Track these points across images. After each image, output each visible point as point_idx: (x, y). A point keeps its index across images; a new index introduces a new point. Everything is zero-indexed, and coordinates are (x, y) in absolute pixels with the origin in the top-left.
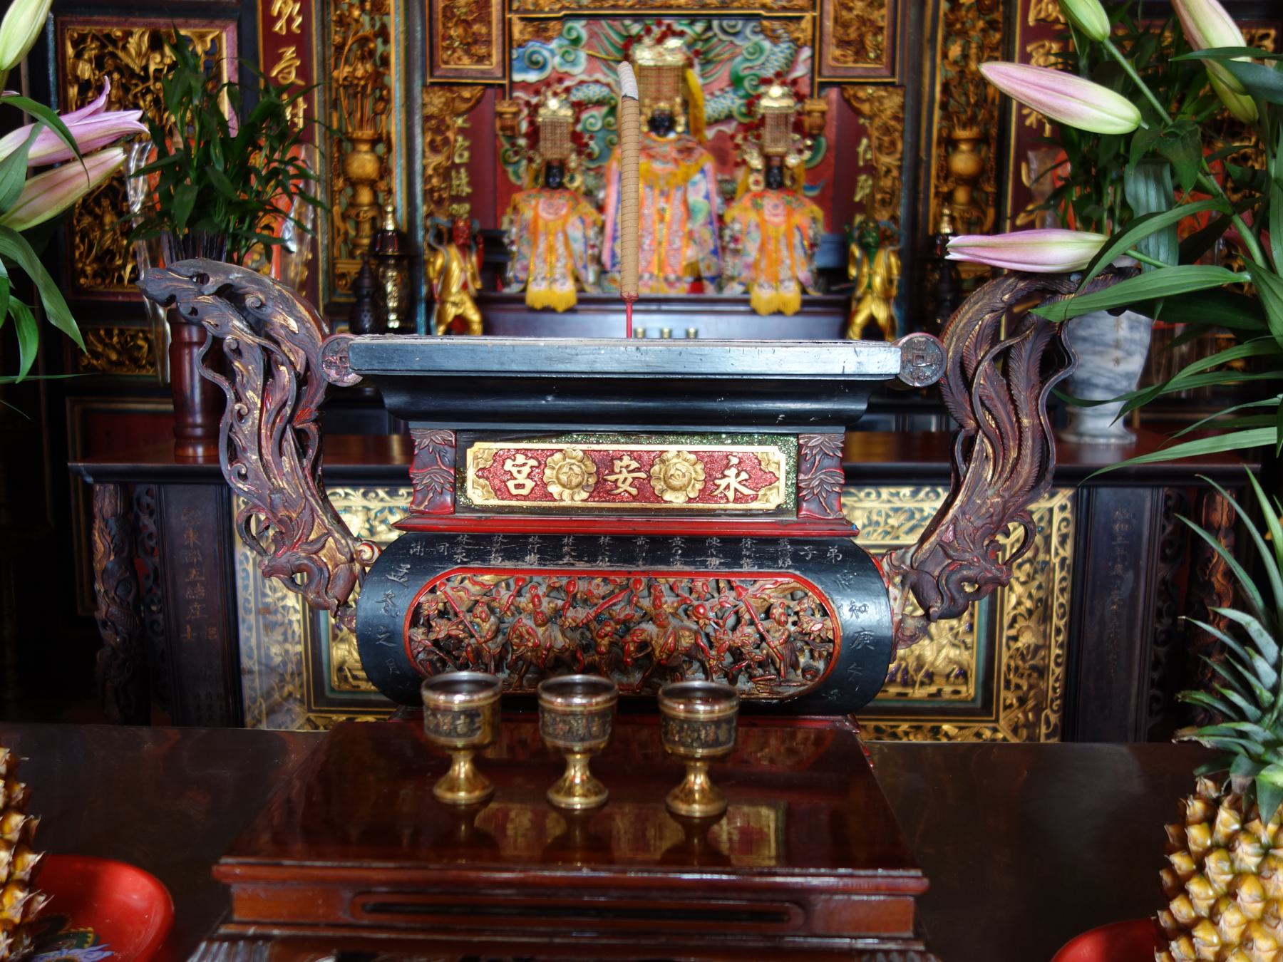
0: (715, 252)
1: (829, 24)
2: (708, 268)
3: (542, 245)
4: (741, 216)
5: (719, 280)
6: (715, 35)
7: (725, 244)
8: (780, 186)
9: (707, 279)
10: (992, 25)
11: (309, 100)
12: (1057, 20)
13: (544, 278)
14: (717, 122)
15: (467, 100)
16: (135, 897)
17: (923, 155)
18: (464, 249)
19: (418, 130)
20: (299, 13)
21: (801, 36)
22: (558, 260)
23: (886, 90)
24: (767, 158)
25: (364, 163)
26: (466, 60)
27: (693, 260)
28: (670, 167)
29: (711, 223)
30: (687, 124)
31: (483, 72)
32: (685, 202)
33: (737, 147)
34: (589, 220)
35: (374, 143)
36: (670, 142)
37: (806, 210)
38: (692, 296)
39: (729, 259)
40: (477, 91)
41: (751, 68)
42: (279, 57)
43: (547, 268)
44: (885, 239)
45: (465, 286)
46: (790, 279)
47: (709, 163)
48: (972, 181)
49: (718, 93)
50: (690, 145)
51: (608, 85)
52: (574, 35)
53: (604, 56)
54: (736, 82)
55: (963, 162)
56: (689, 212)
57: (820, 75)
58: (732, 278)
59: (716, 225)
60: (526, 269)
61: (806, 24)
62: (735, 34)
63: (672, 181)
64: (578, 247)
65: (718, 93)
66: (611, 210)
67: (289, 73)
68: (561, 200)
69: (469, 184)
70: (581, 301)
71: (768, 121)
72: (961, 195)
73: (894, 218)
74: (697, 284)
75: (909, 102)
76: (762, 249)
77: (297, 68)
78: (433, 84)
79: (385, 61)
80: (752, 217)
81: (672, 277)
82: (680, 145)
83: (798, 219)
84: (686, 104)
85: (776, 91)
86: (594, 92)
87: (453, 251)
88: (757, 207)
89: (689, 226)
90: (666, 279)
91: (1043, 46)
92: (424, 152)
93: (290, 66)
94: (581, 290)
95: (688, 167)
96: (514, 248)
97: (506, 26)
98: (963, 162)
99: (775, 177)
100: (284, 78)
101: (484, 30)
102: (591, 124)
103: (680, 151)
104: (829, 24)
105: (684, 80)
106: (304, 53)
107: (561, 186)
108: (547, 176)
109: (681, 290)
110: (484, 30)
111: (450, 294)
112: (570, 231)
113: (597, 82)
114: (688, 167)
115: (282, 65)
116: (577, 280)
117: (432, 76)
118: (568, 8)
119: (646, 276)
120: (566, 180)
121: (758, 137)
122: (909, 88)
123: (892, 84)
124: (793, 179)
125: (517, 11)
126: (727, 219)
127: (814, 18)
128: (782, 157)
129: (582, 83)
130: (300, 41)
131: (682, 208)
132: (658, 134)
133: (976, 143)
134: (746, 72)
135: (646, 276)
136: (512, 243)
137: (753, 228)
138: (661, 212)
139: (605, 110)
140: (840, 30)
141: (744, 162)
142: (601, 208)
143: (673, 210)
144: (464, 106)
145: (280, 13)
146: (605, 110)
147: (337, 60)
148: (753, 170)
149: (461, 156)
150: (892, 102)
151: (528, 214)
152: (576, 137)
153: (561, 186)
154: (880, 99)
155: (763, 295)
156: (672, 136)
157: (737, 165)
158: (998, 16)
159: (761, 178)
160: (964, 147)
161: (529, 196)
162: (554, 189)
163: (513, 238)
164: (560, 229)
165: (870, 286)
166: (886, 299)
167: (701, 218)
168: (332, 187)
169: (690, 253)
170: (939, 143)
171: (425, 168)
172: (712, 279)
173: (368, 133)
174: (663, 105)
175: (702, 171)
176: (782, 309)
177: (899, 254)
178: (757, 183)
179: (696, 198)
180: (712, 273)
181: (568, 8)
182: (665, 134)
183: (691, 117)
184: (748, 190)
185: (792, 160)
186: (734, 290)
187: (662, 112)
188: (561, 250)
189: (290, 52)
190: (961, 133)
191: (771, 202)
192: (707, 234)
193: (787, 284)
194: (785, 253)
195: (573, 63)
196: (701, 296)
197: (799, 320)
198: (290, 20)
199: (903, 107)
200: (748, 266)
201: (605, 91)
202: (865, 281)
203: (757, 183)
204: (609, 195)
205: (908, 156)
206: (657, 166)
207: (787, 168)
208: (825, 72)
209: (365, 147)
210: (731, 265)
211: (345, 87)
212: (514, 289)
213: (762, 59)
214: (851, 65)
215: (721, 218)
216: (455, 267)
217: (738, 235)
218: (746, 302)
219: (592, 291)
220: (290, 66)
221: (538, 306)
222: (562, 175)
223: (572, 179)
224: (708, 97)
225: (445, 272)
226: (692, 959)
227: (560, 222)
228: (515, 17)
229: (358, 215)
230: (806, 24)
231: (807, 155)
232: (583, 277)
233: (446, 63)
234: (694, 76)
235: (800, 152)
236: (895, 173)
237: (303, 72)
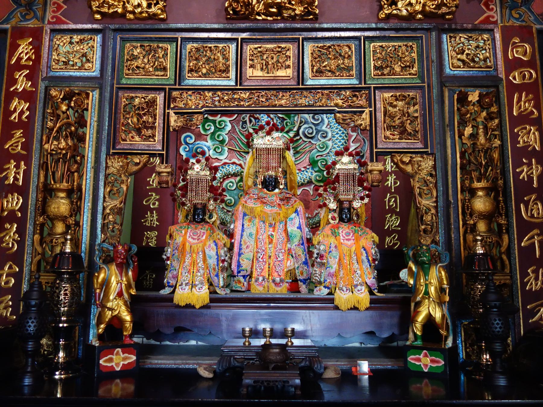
0: (306, 263)
1: (380, 116)
2: (302, 273)
3: (188, 261)
4: (324, 240)
5: (309, 281)
6: (301, 138)
7: (312, 255)
8: (350, 220)
9: (301, 281)
10: (490, 117)
11: (28, 164)
12: (532, 113)
13: (187, 284)
14: (302, 185)
15: (137, 164)
16: (266, 239)
17: (451, 199)
18: (122, 267)
19: (102, 183)
20: (27, 109)
21: (362, 122)
22: (198, 271)
23: (422, 157)
24: (340, 203)
25: (61, 205)
26: (137, 138)
27: (292, 268)
28: (276, 209)
29: (303, 244)
30: (286, 184)
31: (148, 146)
32: (286, 230)
33: (320, 195)
34: (221, 243)
35: (69, 193)
36: (276, 194)
37: (369, 236)
38: (292, 296)
39: (317, 269)
40: (144, 158)
41: (322, 156)
42: (12, 136)
43: (190, 277)
44: (435, 260)
45: (120, 294)
46: (361, 285)
47: (301, 208)
48: (488, 217)
49: (303, 169)
50: (288, 196)
51: (240, 165)
52: (221, 138)
53: (238, 150)
54: (313, 163)
55: (481, 204)
56: (289, 237)
57: (376, 148)
58: (320, 283)
59: (306, 245)
60: (176, 277)
61: (366, 116)
62: (312, 138)
63: (277, 219)
64: (212, 262)
65: (303, 169)
66: (237, 237)
67: (17, 146)
68: (203, 231)
69: (158, 220)
70: (212, 300)
71: (341, 178)
72: (482, 226)
73: (434, 242)
74: (294, 286)
75: (439, 164)
76: (340, 263)
77: (22, 143)
78: (114, 154)
79: (82, 139)
80: (332, 240)
81: (278, 280)
82: (281, 196)
83: (363, 242)
84: (285, 173)
85: (346, 159)
86: (232, 169)
87: (114, 267)
88: (335, 234)
89: (289, 246)
90: (274, 281)
91: (526, 128)
92: (104, 197)
93: (18, 142)
94: (213, 292)
95: (287, 209)
96: (169, 262)
97: (166, 118)
98: (481, 204)
99: (345, 214)
100: (13, 149)
101: (150, 120)
102: (230, 186)
103: (281, 200)
104: (380, 116)
105: (284, 158)
106: (28, 134)
107: (203, 220)
108: (194, 216)
109: (283, 290)
110: (150, 120)
111: (108, 301)
112: (207, 251)
113: (234, 163)
114: (287, 209)
115: (13, 141)
116: (211, 284)
117: (114, 148)
118: (207, 107)
119: (261, 279)
120: (207, 217)
121: (334, 189)
122: (438, 155)
123: (426, 153)
124: (358, 215)
125: (173, 109)
126: (315, 242)
127: (371, 112)
128: (350, 202)
129: (225, 164)
130: (26, 127)
131: (284, 235)
132: (268, 190)
133: (488, 191)
134: (319, 158)
135: (261, 279)
136: (168, 259)
137: (333, 248)
138: (271, 237)
139: (238, 178)
140: (388, 120)
141: (325, 205)
142: (231, 235)
143: (279, 235)
144: (135, 168)
145: (15, 109)
146: (238, 178)
147: (48, 138)
148: (330, 210)
149: (154, 204)
150: (427, 164)
151: (179, 240)
152: (212, 189)
153: (203, 220)
154: (418, 163)
155: (343, 297)
156: (277, 191)
157: (320, 207)
158: (494, 109)
159: (336, 215)
160: (480, 193)
161: (181, 227)
162: (199, 223)
163: (168, 255)
164: (200, 249)
165: (427, 293)
166: (441, 303)
167: (296, 241)
168: (35, 221)
169: (290, 264)
170: (462, 191)
171: (104, 208)
172: (304, 281)
173: (65, 185)
174: (270, 173)
175: (296, 211)
176: (357, 306)
177: (445, 268)
178: (334, 218)
179: (292, 229)
180: (305, 276)
181: (207, 107)
182: (273, 190)
183: (288, 180)
184: (328, 223)
185: (357, 204)
186: (322, 292)
187: (271, 176)
188: (201, 264)
189: (19, 133)
190: (477, 185)
191: (344, 230)
192: (300, 251)
193: (359, 288)
194: (356, 266)
195: (220, 153)
196: (299, 296)
197: (366, 312)
198: (22, 113)
199: (434, 167)
200: (331, 275)
201: (239, 168)
202: (423, 289)
203: (334, 218)
204: (236, 227)
205: (441, 199)
206: (268, 209)
207: (354, 209)
208: (379, 146)
209: (62, 195)
210: (318, 272)
211: (52, 155)
212: (166, 291)
213: (328, 151)
214: (397, 140)
215: (309, 241)
216: (113, 280)
217: (323, 253)
218: (332, 301)
219: (222, 293)
220: (18, 142)
221: (183, 304)
222: (204, 214)
223: (211, 217)
224: (298, 171)
225: (106, 283)
226: (270, 1)
227: (201, 245)
228: (172, 112)
229: (51, 241)
230: (366, 116)
231: (366, 200)
232: (215, 284)
233: (125, 140)
234: (290, 155)
235: (362, 198)
236: (433, 211)
237: (27, 146)
